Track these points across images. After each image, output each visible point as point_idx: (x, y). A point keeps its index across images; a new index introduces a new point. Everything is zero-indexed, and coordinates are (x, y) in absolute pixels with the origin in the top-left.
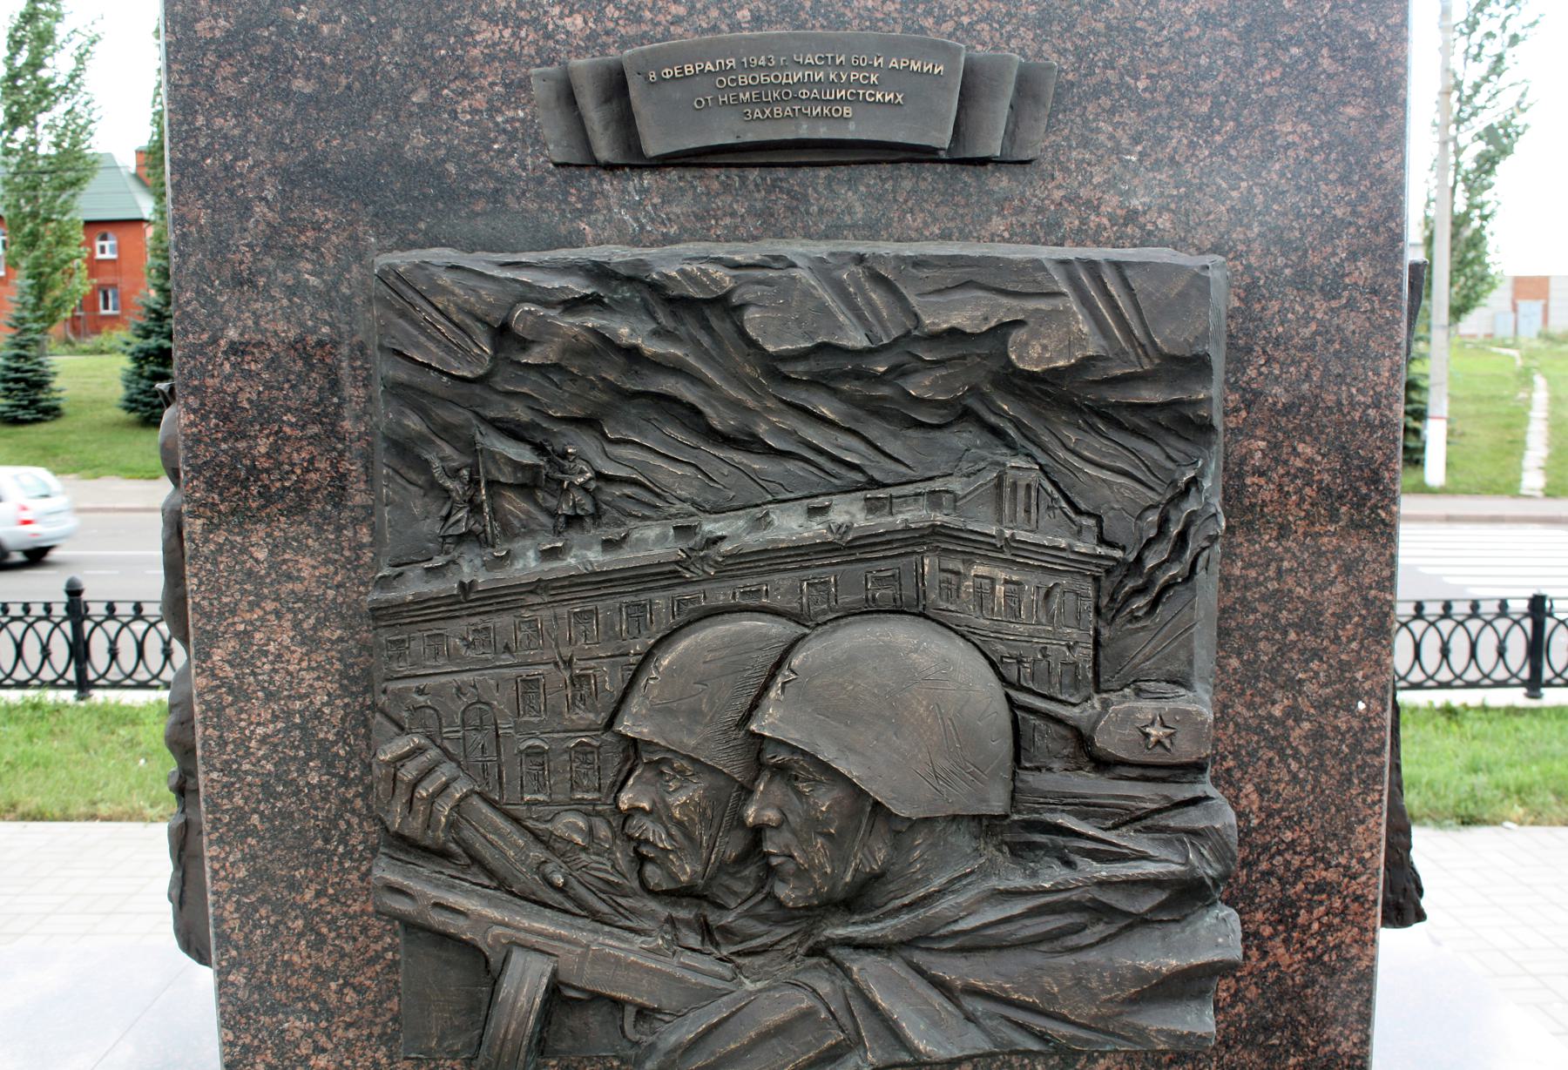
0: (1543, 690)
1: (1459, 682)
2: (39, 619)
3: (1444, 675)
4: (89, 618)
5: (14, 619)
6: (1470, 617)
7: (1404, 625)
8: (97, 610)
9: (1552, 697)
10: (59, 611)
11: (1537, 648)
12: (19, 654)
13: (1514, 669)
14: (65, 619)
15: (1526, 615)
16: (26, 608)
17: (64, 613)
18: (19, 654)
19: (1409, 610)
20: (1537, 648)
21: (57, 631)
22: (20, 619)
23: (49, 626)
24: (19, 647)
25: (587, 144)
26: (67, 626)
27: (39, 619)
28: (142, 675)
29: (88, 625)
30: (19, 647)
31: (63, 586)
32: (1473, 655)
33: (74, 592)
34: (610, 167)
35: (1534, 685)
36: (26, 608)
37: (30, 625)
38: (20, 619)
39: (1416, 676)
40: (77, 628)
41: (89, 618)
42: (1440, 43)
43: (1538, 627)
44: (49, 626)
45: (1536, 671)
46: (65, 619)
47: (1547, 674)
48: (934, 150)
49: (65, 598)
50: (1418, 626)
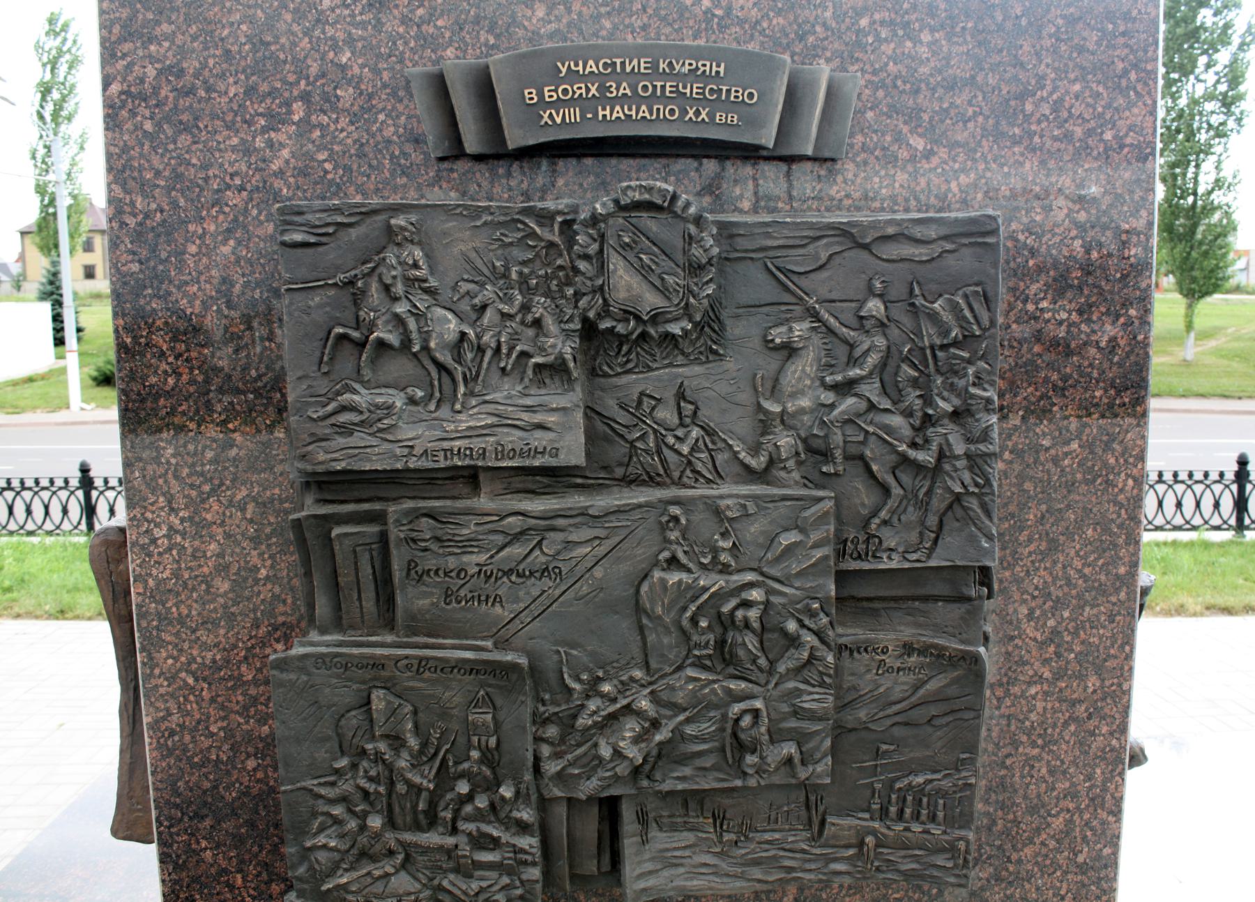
0: (1246, 532)
1: (1188, 526)
2: (60, 488)
3: (1178, 521)
4: (96, 488)
5: (43, 489)
6: (1158, 482)
7: (1151, 486)
8: (99, 483)
9: (1250, 535)
10: (74, 483)
11: (1241, 504)
12: (11, 512)
13: (1225, 518)
14: (78, 488)
15: (1234, 482)
16: (52, 482)
17: (1233, 478)
18: (11, 512)
19: (1153, 477)
20: (1241, 504)
21: (73, 497)
22: (1201, 482)
23: (1222, 487)
24: (11, 509)
25: (457, 140)
26: (80, 494)
27: (60, 488)
28: (30, 526)
29: (94, 494)
30: (11, 509)
31: (78, 466)
32: (47, 507)
33: (85, 470)
34: (479, 158)
35: (1240, 527)
36: (52, 482)
37: (54, 493)
38: (1201, 482)
39: (1159, 521)
40: (88, 496)
41: (96, 488)
42: (31, 214)
43: (1241, 489)
44: (1222, 487)
45: (1240, 520)
46: (78, 488)
47: (1247, 521)
48: (758, 148)
49: (79, 474)
50: (1161, 488)
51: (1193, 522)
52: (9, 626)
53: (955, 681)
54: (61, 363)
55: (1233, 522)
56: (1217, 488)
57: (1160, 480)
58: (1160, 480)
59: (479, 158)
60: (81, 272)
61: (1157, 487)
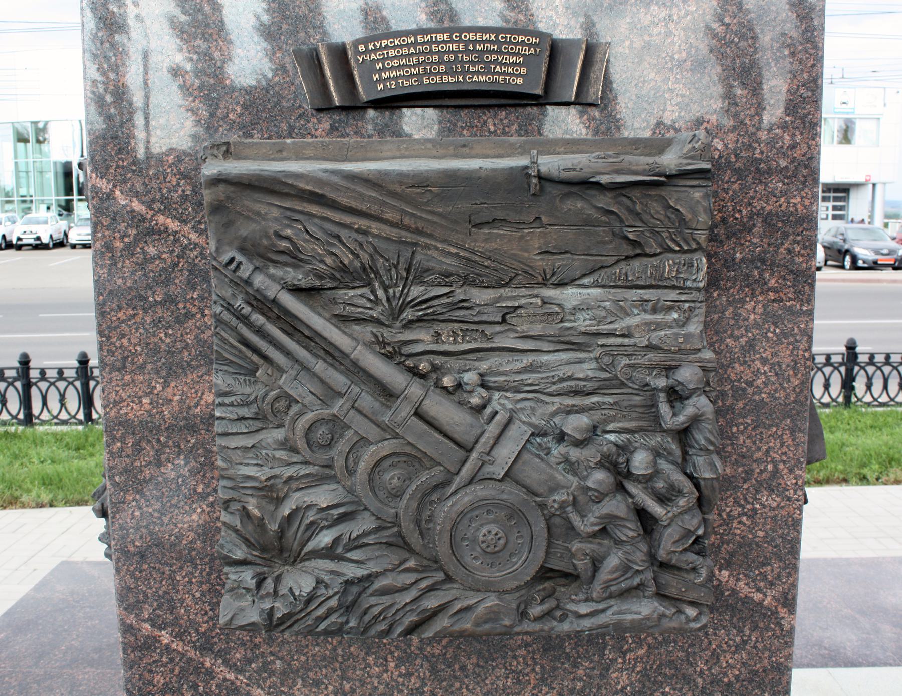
4: (93, 379)
6: (868, 364)
8: (863, 359)
19: (820, 359)
29: (92, 384)
31: (17, 358)
33: (25, 362)
40: (85, 386)
43: (85, 386)
49: (843, 349)
51: (60, 417)
52: (12, 515)
53: (341, 615)
54: (886, 221)
55: (81, 416)
56: (62, 385)
57: (871, 362)
58: (871, 362)
59: (342, 108)
60: (858, 136)
61: (58, 384)
